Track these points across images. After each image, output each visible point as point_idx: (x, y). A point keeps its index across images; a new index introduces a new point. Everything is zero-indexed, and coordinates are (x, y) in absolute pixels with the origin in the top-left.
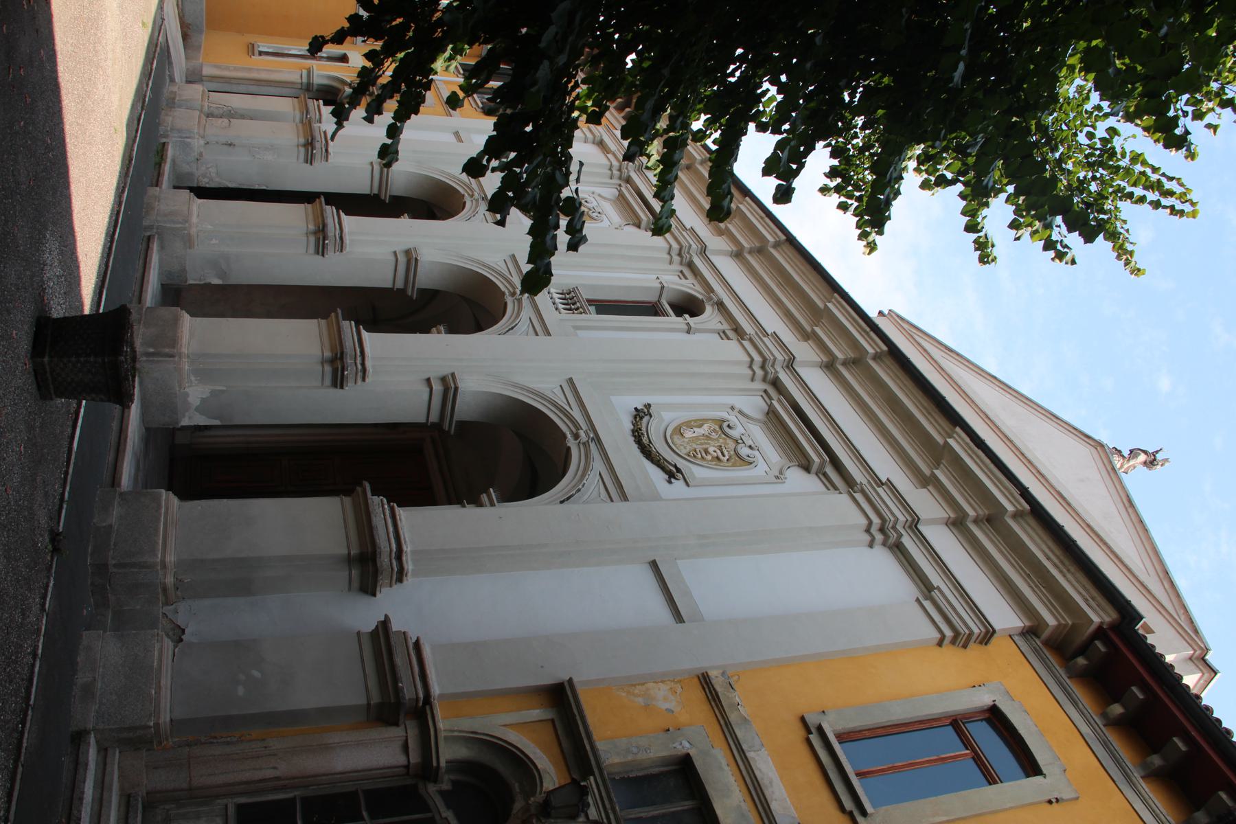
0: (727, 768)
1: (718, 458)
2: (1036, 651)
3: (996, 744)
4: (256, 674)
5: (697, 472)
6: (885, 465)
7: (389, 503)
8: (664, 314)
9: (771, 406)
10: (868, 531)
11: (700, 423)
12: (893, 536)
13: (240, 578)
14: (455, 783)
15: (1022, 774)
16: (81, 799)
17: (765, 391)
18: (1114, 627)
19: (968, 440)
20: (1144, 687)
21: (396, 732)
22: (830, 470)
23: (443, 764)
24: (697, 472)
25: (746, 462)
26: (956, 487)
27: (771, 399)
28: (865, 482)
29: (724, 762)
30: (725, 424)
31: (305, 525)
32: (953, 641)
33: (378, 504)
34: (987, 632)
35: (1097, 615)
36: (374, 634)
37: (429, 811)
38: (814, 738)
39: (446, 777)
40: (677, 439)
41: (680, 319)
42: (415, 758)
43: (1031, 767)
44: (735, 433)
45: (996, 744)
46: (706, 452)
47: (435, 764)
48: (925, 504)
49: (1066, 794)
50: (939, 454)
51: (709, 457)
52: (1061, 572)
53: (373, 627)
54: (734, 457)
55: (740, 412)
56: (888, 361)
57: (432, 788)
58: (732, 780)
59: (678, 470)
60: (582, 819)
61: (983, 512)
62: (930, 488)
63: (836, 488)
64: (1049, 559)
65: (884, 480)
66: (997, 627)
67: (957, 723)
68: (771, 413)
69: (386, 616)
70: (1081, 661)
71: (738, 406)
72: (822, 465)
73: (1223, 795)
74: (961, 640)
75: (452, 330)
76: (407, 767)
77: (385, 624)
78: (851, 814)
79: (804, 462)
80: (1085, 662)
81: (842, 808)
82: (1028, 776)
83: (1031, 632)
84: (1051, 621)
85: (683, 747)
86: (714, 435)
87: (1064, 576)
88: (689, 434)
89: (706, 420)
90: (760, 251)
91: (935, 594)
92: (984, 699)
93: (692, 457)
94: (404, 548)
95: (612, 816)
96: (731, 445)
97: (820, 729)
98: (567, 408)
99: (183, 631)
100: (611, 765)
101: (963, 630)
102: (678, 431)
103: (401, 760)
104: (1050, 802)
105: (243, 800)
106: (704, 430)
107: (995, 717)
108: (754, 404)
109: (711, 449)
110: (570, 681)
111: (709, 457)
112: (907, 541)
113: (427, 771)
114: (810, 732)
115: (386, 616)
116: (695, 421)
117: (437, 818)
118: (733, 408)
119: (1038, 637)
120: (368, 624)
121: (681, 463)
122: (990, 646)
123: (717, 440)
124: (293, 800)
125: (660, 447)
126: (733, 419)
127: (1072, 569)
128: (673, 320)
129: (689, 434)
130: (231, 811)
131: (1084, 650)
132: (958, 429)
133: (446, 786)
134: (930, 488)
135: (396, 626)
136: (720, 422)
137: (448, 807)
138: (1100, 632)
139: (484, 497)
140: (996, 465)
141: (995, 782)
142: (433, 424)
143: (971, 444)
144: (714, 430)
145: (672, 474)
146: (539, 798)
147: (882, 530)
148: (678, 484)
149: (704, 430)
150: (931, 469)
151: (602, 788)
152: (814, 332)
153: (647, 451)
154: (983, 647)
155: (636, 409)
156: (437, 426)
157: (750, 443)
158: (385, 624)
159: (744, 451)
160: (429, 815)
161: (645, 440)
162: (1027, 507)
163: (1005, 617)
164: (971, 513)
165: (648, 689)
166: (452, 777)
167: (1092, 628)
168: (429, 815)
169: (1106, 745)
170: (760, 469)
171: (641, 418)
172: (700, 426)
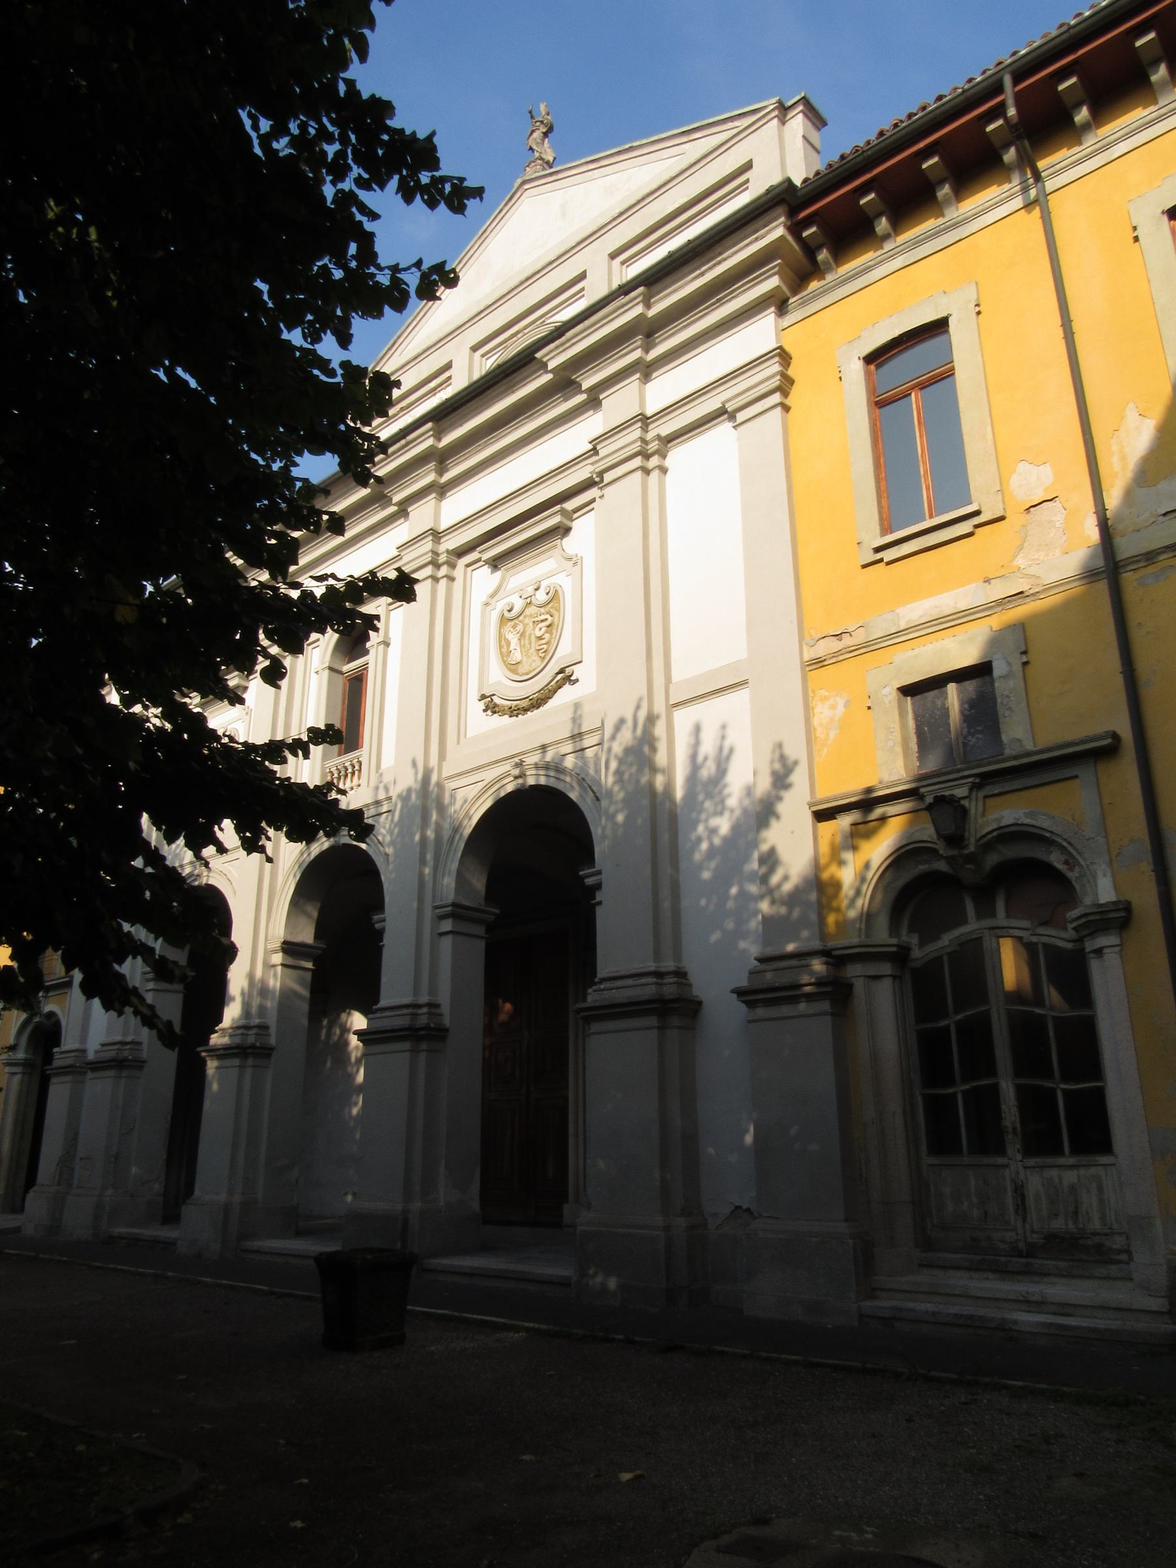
0: (917, 651)
1: (548, 626)
2: (804, 303)
3: (910, 362)
4: (793, 1131)
5: (564, 652)
6: (573, 440)
7: (595, 984)
8: (365, 668)
9: (486, 562)
10: (647, 472)
11: (502, 641)
12: (653, 446)
13: (680, 1145)
14: (911, 930)
15: (943, 338)
16: (934, 1314)
17: (468, 566)
18: (792, 213)
19: (552, 346)
20: (863, 190)
21: (859, 986)
22: (570, 505)
23: (894, 941)
24: (564, 652)
25: (554, 597)
26: (720, 303)
27: (479, 560)
28: (591, 468)
29: (910, 653)
30: (507, 615)
31: (612, 1071)
32: (786, 394)
33: (593, 997)
34: (779, 355)
35: (776, 231)
36: (751, 1004)
37: (941, 957)
38: (888, 555)
39: (904, 938)
40: (521, 670)
41: (372, 652)
42: (886, 968)
43: (939, 327)
44: (519, 605)
45: (910, 362)
46: (540, 638)
47: (894, 949)
48: (621, 403)
49: (971, 294)
50: (564, 383)
51: (547, 636)
52: (719, 263)
53: (743, 1006)
54: (548, 608)
55: (493, 596)
56: (446, 422)
57: (916, 953)
58: (929, 647)
59: (562, 671)
60: (965, 803)
61: (639, 340)
62: (601, 397)
63: (593, 500)
64: (702, 274)
65: (590, 447)
66: (774, 345)
67: (880, 403)
68: (495, 563)
69: (733, 991)
70: (823, 255)
71: (484, 599)
72: (563, 512)
73: (990, 128)
74: (785, 385)
75: (379, 906)
76: (894, 977)
77: (740, 993)
78: (977, 526)
79: (561, 530)
80: (884, 220)
81: (971, 534)
82: (947, 331)
83: (782, 308)
84: (774, 282)
85: (890, 694)
86: (520, 627)
87: (725, 260)
88: (517, 656)
89: (501, 636)
90: (442, 458)
91: (730, 407)
92: (855, 369)
93: (546, 654)
94: (652, 969)
95: (966, 773)
96: (532, 610)
97: (878, 550)
98: (481, 785)
99: (738, 1208)
100: (906, 768)
101: (636, 447)
102: (513, 667)
103: (887, 983)
104: (979, 313)
105: (924, 1148)
106: (513, 638)
107: (875, 358)
108: (482, 580)
109: (539, 634)
110: (810, 805)
111: (547, 636)
112: (666, 428)
113: (900, 957)
114: (881, 560)
115: (733, 991)
116: (501, 647)
117: (949, 950)
118: (487, 604)
119: (787, 300)
120: (739, 1009)
121: (553, 667)
122: (793, 355)
123: (525, 626)
124: (924, 1096)
125: (532, 688)
126: (500, 605)
127: (719, 250)
128: (372, 659)
129: (517, 656)
130: (934, 1160)
131: (810, 250)
132: (538, 355)
133: (914, 940)
134: (601, 397)
135: (743, 982)
136: (503, 620)
137: (937, 938)
138: (795, 229)
139: (589, 881)
140: (586, 318)
141: (953, 369)
142: (487, 931)
143: (557, 342)
144: (514, 627)
145: (566, 678)
146: (941, 848)
147: (647, 456)
148: (578, 672)
149: (513, 638)
150: (581, 392)
151: (941, 779)
152: (400, 504)
153: (537, 703)
154: (793, 362)
155: (485, 711)
156: (490, 928)
157: (531, 590)
158: (740, 993)
159: (541, 597)
160: (945, 958)
161: (525, 703)
162: (641, 289)
163: (762, 333)
164: (638, 354)
165: (821, 724)
166: (904, 931)
167: (789, 238)
168: (945, 958)
169: (918, 242)
170: (564, 582)
171: (496, 705)
172: (508, 643)
